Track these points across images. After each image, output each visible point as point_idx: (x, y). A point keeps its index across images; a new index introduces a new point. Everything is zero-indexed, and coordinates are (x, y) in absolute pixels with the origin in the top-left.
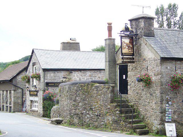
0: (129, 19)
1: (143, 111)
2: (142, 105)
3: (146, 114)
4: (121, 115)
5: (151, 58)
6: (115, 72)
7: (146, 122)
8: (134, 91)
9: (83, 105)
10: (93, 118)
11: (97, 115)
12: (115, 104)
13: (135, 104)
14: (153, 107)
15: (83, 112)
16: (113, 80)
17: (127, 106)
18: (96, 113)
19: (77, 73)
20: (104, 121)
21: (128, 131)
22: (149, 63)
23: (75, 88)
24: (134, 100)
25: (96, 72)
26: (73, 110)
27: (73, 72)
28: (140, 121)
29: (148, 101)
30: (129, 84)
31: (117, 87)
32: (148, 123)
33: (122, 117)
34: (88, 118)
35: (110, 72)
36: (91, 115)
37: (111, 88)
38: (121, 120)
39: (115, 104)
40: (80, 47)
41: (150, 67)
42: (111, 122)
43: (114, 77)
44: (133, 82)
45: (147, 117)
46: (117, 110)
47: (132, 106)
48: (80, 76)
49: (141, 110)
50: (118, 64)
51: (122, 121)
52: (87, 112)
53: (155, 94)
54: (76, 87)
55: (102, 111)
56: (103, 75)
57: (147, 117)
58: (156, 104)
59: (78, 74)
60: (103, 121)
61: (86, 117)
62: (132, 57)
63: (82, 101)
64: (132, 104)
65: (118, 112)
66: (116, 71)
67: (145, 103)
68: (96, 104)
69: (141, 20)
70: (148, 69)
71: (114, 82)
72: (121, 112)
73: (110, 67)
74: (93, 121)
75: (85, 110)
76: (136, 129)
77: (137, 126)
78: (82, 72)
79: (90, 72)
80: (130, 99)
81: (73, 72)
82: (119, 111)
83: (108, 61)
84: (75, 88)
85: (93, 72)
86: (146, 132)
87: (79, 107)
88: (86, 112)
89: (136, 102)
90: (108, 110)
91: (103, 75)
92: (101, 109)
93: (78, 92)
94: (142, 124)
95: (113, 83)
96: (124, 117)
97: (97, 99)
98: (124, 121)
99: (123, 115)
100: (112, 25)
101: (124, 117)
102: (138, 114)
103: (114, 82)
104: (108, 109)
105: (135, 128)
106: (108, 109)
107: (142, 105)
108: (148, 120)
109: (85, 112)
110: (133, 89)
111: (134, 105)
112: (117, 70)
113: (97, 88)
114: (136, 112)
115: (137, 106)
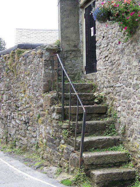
2: (122, 94)
3: (130, 123)
4: (60, 124)
6: (77, 25)
7: (130, 144)
8: (107, 59)
12: (54, 94)
13: (109, 93)
16: (72, 44)
17: (89, 98)
20: (36, 137)
21: (73, 172)
24: (106, 84)
28: (116, 143)
29: (135, 82)
30: (97, 45)
31: (82, 59)
32: (134, 149)
33: (62, 129)
34: (13, 127)
35: (64, 24)
36: (17, 121)
37: (47, 54)
38: (60, 139)
39: (54, 94)
43: (74, 36)
44: (104, 37)
45: (133, 131)
46: (53, 111)
47: (101, 101)
49: (119, 109)
51: (63, 141)
55: (31, 113)
57: (133, 131)
64: (102, 94)
65: (54, 115)
66: (78, 21)
67: (128, 88)
71: (75, 46)
72: (64, 115)
73: (65, 13)
76: (93, 169)
77: (98, 157)
80: (100, 81)
82: (58, 113)
86: (126, 178)
89: (110, 87)
92: (30, 107)
94: (121, 151)
95: (73, 49)
96: (66, 129)
97: (24, 84)
98: (66, 142)
99: (65, 125)
101: (66, 129)
102: (113, 122)
103: (75, 46)
105: (92, 164)
107: (122, 94)
108: (135, 139)
110: (105, 53)
111: (107, 97)
112: (80, 21)
113: (25, 59)
114: (110, 116)
115: (111, 99)
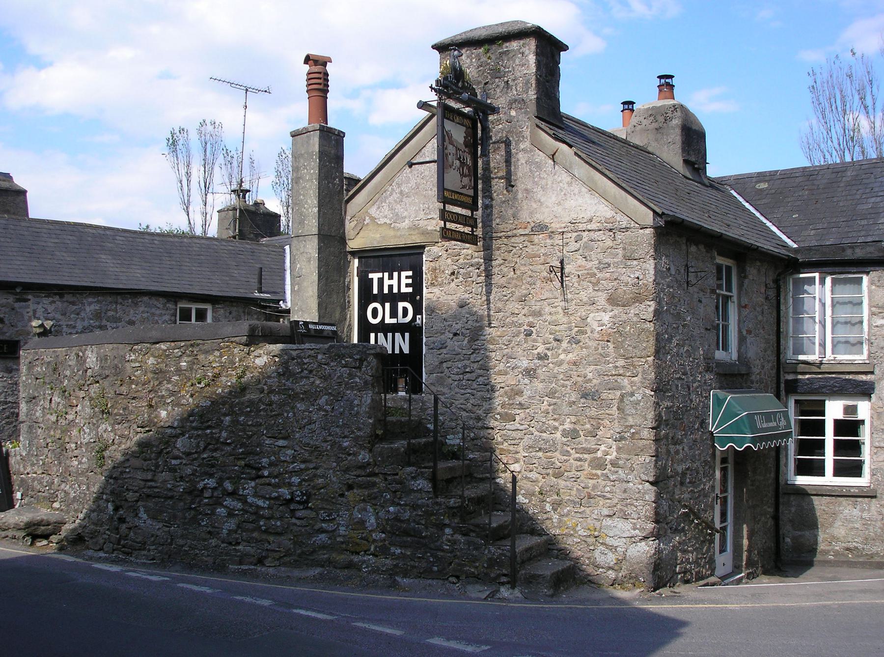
0: (433, 43)
1: (533, 475)
5: (591, 221)
9: (198, 446)
10: (263, 517)
11: (289, 502)
14: (599, 454)
15: (201, 485)
18: (285, 492)
19: (46, 301)
22: (573, 246)
23: (151, 361)
25: (120, 300)
26: (140, 475)
27: (30, 297)
29: (567, 426)
34: (231, 514)
36: (250, 500)
40: (29, 206)
41: (581, 261)
42: (378, 536)
48: (58, 316)
50: (354, 253)
52: (229, 486)
53: (618, 393)
54: (159, 356)
56: (145, 315)
58: (622, 439)
59: (51, 308)
60: (322, 531)
61: (221, 511)
62: (466, 212)
63: (196, 429)
68: (281, 443)
69: (514, 45)
70: (566, 271)
74: (266, 532)
75: (211, 476)
77: (850, 603)
78: (65, 299)
79: (98, 302)
81: (30, 297)
83: (315, 230)
84: (151, 361)
85: (109, 299)
87: (176, 458)
88: (220, 482)
90: (358, 472)
91: (145, 315)
92: (316, 468)
93: (169, 382)
100: (329, 68)
104: (360, 467)
106: (360, 467)
109: (211, 482)
